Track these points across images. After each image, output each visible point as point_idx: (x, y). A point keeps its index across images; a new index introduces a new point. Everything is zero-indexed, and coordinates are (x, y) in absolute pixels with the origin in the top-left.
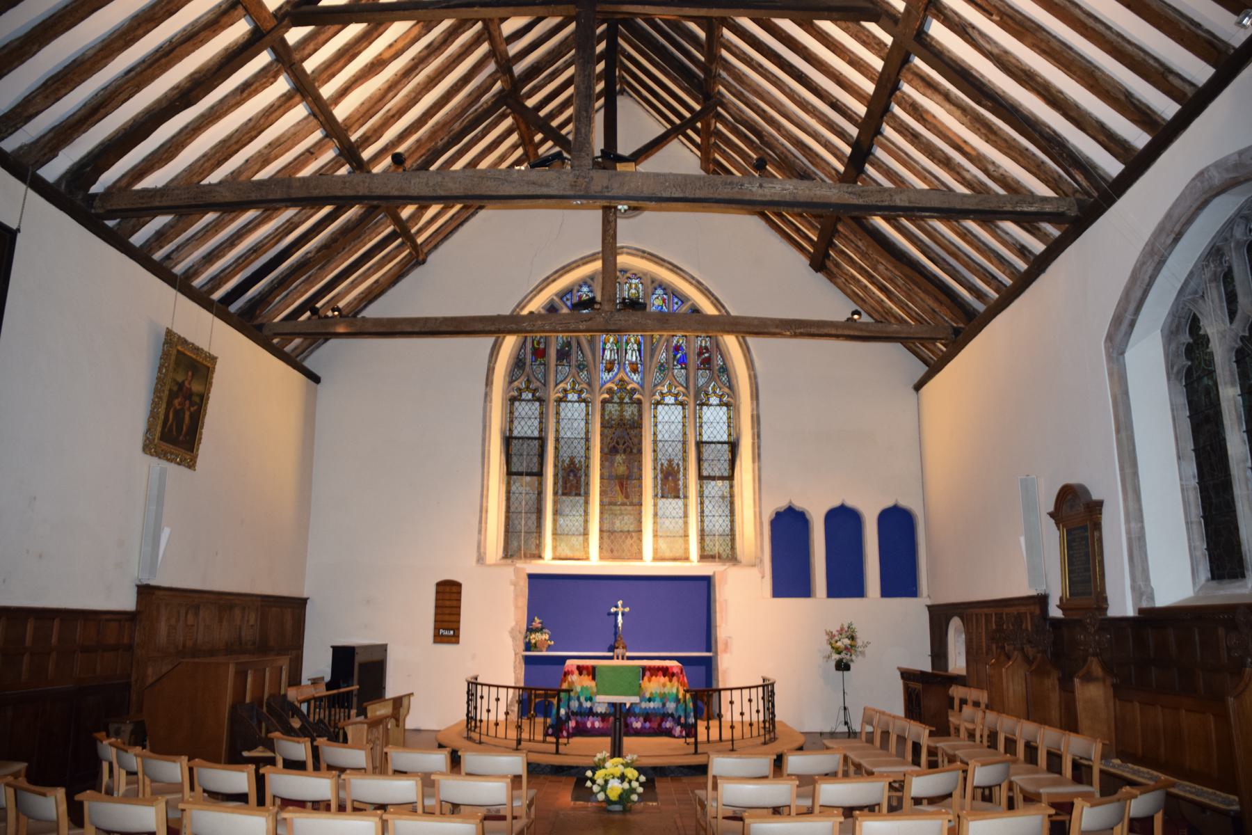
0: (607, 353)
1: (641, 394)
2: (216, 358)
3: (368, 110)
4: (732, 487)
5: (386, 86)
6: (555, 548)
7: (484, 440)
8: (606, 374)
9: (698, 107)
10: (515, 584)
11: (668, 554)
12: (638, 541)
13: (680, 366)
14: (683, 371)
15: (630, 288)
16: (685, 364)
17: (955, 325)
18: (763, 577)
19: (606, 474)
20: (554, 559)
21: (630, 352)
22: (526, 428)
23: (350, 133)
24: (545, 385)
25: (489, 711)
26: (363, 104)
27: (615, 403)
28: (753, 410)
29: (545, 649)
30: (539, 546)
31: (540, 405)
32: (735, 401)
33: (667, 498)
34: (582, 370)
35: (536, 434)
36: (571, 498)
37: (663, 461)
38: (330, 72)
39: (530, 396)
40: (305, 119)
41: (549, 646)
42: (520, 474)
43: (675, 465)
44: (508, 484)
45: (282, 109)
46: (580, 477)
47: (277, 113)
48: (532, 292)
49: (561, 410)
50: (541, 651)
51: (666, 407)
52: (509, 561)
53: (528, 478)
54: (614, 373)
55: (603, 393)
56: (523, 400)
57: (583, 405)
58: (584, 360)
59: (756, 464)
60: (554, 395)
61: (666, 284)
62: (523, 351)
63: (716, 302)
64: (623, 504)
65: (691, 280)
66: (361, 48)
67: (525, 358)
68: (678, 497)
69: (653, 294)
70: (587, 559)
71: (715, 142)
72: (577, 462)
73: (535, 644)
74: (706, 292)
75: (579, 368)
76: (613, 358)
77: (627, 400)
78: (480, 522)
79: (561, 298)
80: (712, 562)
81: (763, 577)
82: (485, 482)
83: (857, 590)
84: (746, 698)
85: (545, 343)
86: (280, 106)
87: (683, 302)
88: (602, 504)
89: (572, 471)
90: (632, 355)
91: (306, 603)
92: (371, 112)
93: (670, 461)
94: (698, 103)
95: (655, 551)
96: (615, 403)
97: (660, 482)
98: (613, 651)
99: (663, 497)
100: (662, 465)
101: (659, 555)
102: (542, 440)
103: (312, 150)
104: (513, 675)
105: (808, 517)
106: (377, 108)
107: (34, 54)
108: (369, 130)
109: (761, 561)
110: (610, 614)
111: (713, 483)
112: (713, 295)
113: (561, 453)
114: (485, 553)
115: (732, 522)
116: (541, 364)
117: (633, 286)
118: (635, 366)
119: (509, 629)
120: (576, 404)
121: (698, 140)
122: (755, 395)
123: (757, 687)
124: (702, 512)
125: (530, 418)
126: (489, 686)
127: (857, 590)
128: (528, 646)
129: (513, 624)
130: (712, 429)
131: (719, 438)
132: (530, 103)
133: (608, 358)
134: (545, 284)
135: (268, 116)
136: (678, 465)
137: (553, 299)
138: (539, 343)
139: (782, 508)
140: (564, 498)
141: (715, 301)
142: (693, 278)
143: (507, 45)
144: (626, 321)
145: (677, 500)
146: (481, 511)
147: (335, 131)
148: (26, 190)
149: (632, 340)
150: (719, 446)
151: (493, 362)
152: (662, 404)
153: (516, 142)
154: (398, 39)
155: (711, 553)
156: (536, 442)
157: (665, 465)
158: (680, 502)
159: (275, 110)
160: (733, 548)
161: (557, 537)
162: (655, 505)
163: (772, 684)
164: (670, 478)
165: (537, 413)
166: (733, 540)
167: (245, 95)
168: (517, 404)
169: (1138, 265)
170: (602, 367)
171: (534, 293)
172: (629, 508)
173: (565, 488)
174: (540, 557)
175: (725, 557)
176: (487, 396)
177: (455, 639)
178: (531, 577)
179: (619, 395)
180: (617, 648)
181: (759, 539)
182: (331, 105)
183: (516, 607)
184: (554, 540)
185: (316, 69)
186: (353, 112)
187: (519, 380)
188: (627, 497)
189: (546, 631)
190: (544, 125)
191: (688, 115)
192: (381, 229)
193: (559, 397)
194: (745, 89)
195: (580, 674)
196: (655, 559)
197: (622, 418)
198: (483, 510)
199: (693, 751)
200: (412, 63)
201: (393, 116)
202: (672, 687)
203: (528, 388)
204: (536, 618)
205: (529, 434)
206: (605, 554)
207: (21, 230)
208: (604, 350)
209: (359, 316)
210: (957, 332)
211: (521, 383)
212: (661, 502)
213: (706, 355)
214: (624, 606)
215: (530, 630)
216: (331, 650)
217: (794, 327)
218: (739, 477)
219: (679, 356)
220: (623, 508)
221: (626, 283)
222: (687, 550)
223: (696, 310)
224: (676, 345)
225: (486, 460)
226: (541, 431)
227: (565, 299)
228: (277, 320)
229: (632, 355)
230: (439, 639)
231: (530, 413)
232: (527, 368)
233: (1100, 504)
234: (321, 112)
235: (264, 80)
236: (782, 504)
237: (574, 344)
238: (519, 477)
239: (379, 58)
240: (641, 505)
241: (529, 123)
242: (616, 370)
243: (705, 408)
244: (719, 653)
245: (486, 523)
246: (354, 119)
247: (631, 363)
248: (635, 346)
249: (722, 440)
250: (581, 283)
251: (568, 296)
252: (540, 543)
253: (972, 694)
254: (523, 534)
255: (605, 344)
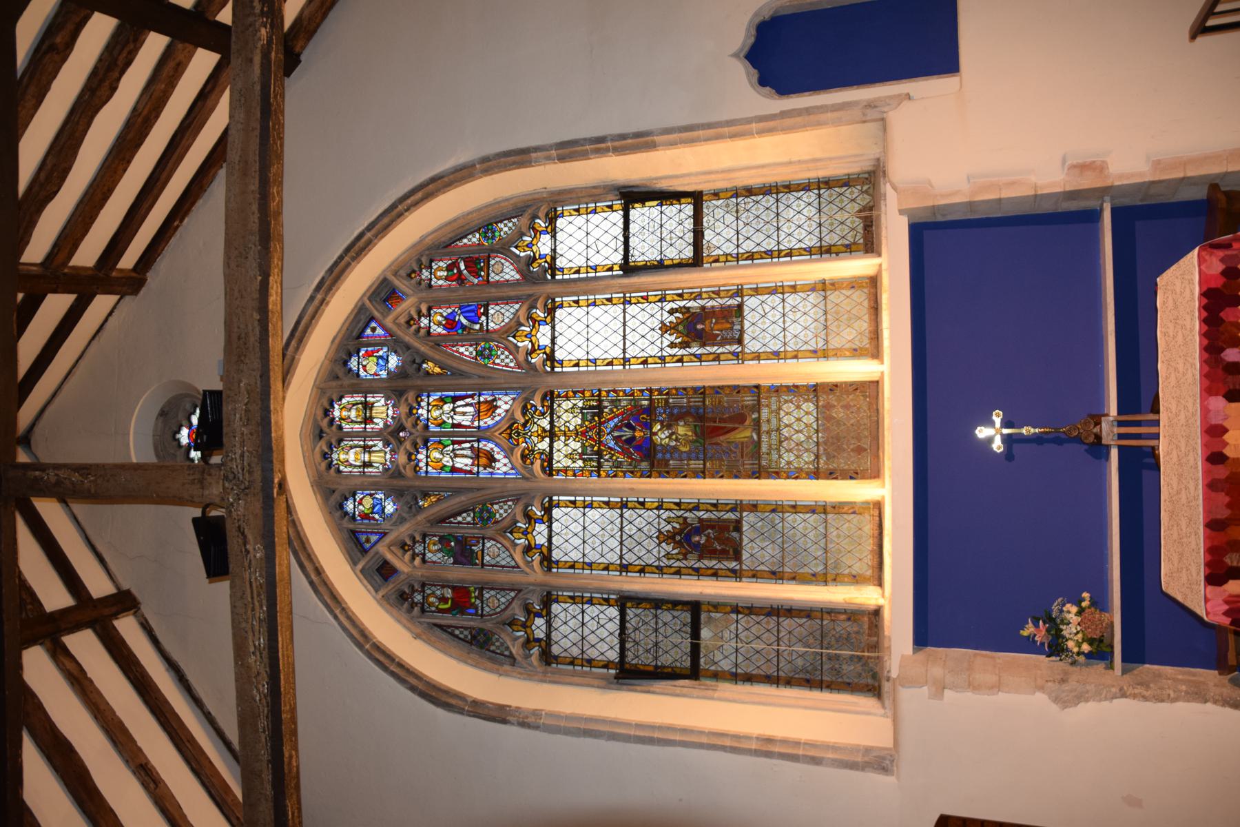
0: (461, 463)
1: (534, 392)
4: (716, 195)
6: (856, 579)
7: (613, 737)
8: (498, 465)
10: (940, 688)
11: (864, 325)
12: (837, 392)
13: (483, 318)
14: (491, 312)
15: (347, 419)
16: (479, 307)
19: (696, 464)
20: (880, 583)
21: (458, 419)
22: (603, 633)
24: (520, 591)
27: (551, 446)
28: (549, 158)
29: (1106, 616)
30: (853, 614)
31: (557, 601)
32: (542, 200)
33: (742, 331)
34: (491, 514)
35: (613, 612)
36: (745, 541)
37: (666, 343)
39: (539, 622)
41: (1094, 603)
42: (695, 650)
43: (672, 319)
44: (716, 676)
46: (700, 520)
48: (336, 617)
49: (566, 558)
50: (1112, 625)
51: (559, 341)
52: (886, 687)
53: (705, 633)
54: (496, 449)
55: (531, 472)
56: (548, 635)
57: (556, 513)
58: (473, 510)
59: (657, 139)
60: (535, 574)
61: (337, 351)
62: (457, 632)
64: (757, 424)
65: (316, 302)
67: (471, 628)
68: (740, 307)
69: (358, 375)
70: (878, 506)
72: (669, 527)
73: (1091, 642)
74: (337, 271)
75: (489, 518)
76: (468, 452)
78: (794, 758)
79: (365, 551)
80: (879, 226)
81: (908, 97)
82: (705, 740)
85: (443, 587)
87: (372, 319)
88: (757, 474)
89: (688, 537)
90: (464, 414)
93: (665, 328)
95: (856, 353)
96: (551, 446)
97: (710, 349)
98: (1108, 447)
99: (740, 342)
100: (672, 345)
101: (866, 342)
102: (624, 602)
104: (1180, 705)
105: (767, 15)
109: (870, 105)
110: (1009, 454)
111: (708, 235)
112: (341, 258)
113: (650, 560)
114: (868, 750)
115: (789, 188)
116: (480, 597)
117: (345, 413)
118: (483, 408)
119: (1054, 708)
120: (555, 526)
122: (520, 157)
124: (769, 254)
125: (583, 624)
128: (1100, 652)
129: (1041, 697)
130: (601, 245)
131: (618, 231)
133: (469, 461)
134: (322, 589)
136: (671, 312)
137: (361, 571)
138: (443, 600)
139: (748, 73)
140: (745, 555)
141: (352, 253)
142: (312, 298)
144: (243, 444)
145: (746, 310)
146: (768, 754)
149: (435, 413)
150: (633, 228)
151: (460, 703)
152: (553, 351)
153: (48, 650)
155: (860, 229)
156: (630, 613)
157: (672, 338)
158: (751, 302)
160: (847, 182)
161: (832, 572)
162: (757, 357)
164: (700, 327)
165: (574, 609)
166: (828, 183)
168: (555, 650)
170: (484, 474)
171: (337, 612)
172: (765, 413)
173: (722, 555)
174: (877, 613)
175: (868, 198)
176: (527, 721)
178: (923, 637)
180: (1098, 437)
181: (823, 117)
183: (997, 687)
184: (836, 580)
187: (509, 644)
188: (740, 419)
189: (1055, 608)
193: (541, 563)
196: (874, 350)
197: (580, 434)
198: (767, 748)
203: (525, 626)
204: (1025, 633)
205: (614, 626)
206: (868, 462)
208: (454, 470)
211: (513, 641)
212: (752, 346)
213: (462, 267)
214: (990, 440)
215: (1056, 647)
217: (251, 19)
218: (686, 180)
219: (464, 321)
220: (764, 427)
221: (340, 428)
222: (853, 283)
224: (445, 327)
225: (657, 735)
226: (607, 601)
227: (367, 546)
229: (464, 414)
231: (572, 623)
232: (488, 626)
236: (741, 75)
237: (444, 529)
238: (703, 652)
240: (757, 387)
242: (491, 445)
243: (560, 263)
244: (1108, 183)
245: (797, 743)
247: (478, 415)
248: (448, 407)
249: (621, 224)
250: (338, 514)
251: (363, 538)
252: (845, 612)
254: (824, 651)
255: (443, 468)
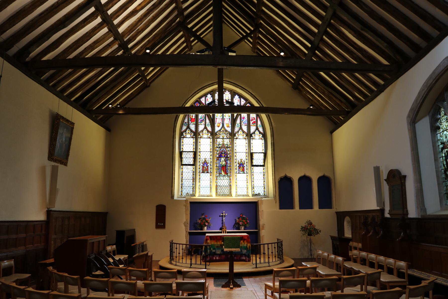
2: (74, 123)
3: (131, 29)
5: (138, 20)
9: (252, 29)
17: (347, 110)
18: (276, 202)
23: (124, 38)
25: (179, 253)
26: (129, 27)
38: (117, 15)
40: (107, 32)
45: (99, 29)
47: (97, 31)
63: (258, 101)
65: (248, 93)
66: (129, 6)
71: (258, 42)
72: (207, 160)
77: (225, 137)
81: (276, 202)
83: (310, 206)
84: (273, 246)
86: (98, 28)
91: (365, 265)
92: (132, 30)
94: (252, 27)
100: (238, 161)
103: (110, 44)
106: (133, 29)
107: (6, 7)
108: (131, 37)
118: (228, 125)
119: (184, 222)
121: (251, 41)
123: (275, 243)
126: (179, 244)
127: (310, 206)
132: (189, 26)
135: (94, 32)
143: (182, 5)
147: (118, 37)
148: (3, 61)
154: (142, 2)
159: (97, 29)
163: (282, 242)
167: (85, 23)
169: (421, 90)
177: (163, 227)
179: (222, 135)
182: (117, 27)
185: (112, 13)
186: (125, 30)
190: (194, 34)
191: (249, 32)
192: (133, 74)
194: (271, 22)
195: (211, 240)
199: (255, 267)
200: (147, 11)
201: (140, 32)
202: (244, 244)
207: (2, 76)
209: (124, 107)
210: (348, 112)
216: (116, 231)
223: (252, 105)
228: (94, 109)
230: (158, 227)
233: (405, 177)
234: (113, 30)
235: (93, 18)
239: (135, 9)
241: (189, 33)
244: (260, 230)
246: (126, 33)
253: (354, 244)
